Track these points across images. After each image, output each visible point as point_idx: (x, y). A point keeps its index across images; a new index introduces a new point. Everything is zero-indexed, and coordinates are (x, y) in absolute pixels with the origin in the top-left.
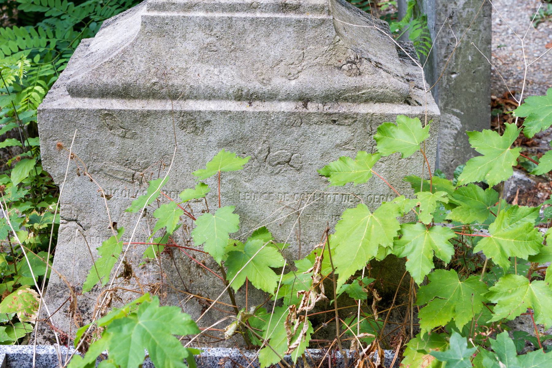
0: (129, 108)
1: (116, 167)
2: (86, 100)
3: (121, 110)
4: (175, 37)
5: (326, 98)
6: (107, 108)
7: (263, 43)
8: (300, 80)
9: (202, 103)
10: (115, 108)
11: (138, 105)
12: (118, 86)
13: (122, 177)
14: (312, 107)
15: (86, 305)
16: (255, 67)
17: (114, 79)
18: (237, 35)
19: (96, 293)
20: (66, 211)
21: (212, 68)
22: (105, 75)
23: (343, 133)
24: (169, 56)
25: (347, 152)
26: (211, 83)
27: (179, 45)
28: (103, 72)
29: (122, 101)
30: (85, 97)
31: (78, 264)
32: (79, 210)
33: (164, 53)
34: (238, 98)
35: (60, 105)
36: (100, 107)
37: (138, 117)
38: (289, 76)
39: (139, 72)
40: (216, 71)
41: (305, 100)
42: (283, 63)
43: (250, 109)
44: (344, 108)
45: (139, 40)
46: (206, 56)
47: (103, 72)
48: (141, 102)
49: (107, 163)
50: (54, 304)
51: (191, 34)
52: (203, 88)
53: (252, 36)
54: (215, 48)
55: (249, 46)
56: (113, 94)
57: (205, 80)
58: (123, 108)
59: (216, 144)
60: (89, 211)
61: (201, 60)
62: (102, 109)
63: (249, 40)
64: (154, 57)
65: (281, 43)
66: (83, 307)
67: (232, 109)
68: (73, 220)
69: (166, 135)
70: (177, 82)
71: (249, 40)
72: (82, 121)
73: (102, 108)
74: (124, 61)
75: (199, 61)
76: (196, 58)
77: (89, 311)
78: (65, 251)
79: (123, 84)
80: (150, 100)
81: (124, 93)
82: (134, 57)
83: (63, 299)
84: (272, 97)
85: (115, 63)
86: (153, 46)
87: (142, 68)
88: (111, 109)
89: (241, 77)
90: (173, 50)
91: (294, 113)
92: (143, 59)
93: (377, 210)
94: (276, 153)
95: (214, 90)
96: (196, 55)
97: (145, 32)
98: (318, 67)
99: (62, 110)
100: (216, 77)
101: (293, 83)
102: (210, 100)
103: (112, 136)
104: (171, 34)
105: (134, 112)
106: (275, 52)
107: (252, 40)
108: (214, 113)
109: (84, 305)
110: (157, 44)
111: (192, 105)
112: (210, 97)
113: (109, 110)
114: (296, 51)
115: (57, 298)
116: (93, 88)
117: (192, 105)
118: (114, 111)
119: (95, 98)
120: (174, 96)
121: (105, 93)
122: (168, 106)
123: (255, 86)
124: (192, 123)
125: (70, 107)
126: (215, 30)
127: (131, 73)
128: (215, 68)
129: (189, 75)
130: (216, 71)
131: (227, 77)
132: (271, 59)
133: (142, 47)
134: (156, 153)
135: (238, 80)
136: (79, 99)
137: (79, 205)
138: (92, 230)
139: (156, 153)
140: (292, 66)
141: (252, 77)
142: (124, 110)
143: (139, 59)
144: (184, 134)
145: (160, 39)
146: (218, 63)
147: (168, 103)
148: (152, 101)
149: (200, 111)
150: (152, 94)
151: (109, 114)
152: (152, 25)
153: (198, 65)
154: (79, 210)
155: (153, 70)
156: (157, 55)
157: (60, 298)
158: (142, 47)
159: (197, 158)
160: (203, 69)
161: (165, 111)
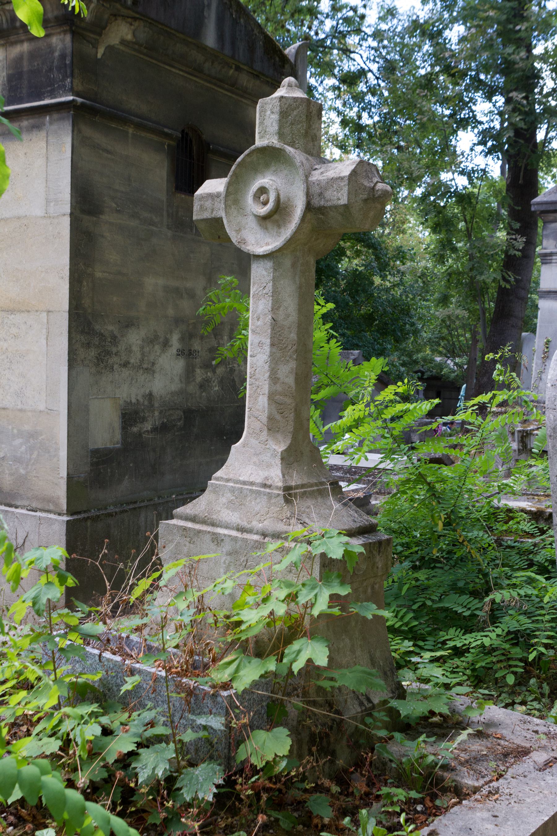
7: (253, 503)
11: (197, 527)
34: (238, 530)
61: (227, 508)
70: (214, 517)
89: (240, 518)
106: (257, 508)
112: (227, 527)
120: (213, 525)
123: (245, 524)
124: (217, 540)
131: (233, 517)
135: (238, 520)
146: (234, 510)
150: (204, 522)
156: (211, 502)
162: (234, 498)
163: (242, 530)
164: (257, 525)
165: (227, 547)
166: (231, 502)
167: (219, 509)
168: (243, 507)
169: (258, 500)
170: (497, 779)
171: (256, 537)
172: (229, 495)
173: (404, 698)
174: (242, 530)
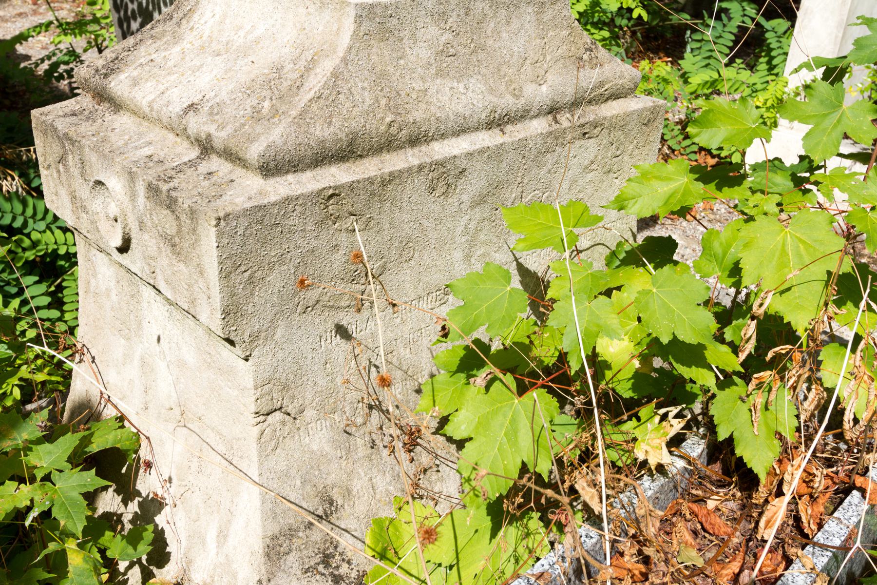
0: (363, 177)
1: (341, 287)
2: (290, 177)
3: (353, 182)
4: (402, 39)
5: (575, 104)
6: (332, 184)
7: (505, 35)
8: (550, 83)
9: (450, 144)
10: (344, 182)
11: (369, 168)
12: (341, 140)
13: (347, 303)
14: (564, 119)
15: (331, 543)
16: (502, 73)
17: (332, 129)
18: (475, 25)
19: (338, 515)
20: (263, 400)
21: (455, 84)
22: (318, 124)
23: (590, 149)
24: (398, 74)
25: (592, 174)
26: (460, 108)
27: (409, 51)
28: (311, 118)
29: (344, 166)
30: (287, 172)
31: (298, 482)
32: (285, 387)
33: (392, 70)
34: (490, 125)
35: (250, 198)
36: (320, 186)
37: (375, 187)
38: (539, 81)
39: (366, 108)
40: (461, 86)
41: (553, 111)
42: (528, 62)
43: (507, 139)
44: (592, 113)
45: (354, 51)
46: (445, 65)
47: (311, 118)
48: (372, 162)
49: (327, 285)
50: (284, 571)
51: (422, 30)
52: (452, 117)
53: (492, 25)
54: (452, 51)
55: (490, 42)
56: (332, 156)
57: (453, 105)
58: (355, 179)
59: (469, 204)
60: (300, 382)
61: (440, 73)
62: (324, 189)
63: (489, 32)
64: (380, 78)
65: (523, 31)
66: (328, 548)
67: (487, 143)
68: (275, 410)
69: (414, 205)
70: (418, 115)
71: (489, 32)
72: (294, 219)
73: (323, 186)
74: (339, 93)
75: (437, 74)
76: (433, 71)
77: (338, 549)
78: (273, 471)
79: (347, 135)
80: (384, 155)
81: (347, 152)
82: (352, 81)
83: (294, 553)
84: (524, 115)
85: (327, 99)
86: (375, 58)
87: (368, 102)
88: (338, 184)
89: (491, 90)
90: (402, 62)
91: (551, 133)
92: (366, 84)
93: (217, 279)
94: (529, 197)
95: (465, 118)
96: (432, 65)
97: (361, 34)
98: (562, 61)
99: (260, 208)
100: (463, 97)
101: (544, 88)
102: (458, 135)
103: (337, 234)
104: (396, 33)
105: (371, 181)
106: (518, 47)
107: (492, 32)
108: (471, 154)
109: (328, 544)
110: (379, 53)
111: (440, 150)
112: (462, 131)
113: (335, 188)
114: (538, 41)
115: (284, 558)
116: (302, 153)
117: (440, 150)
118: (342, 186)
119: (303, 170)
120: (414, 141)
121: (321, 158)
122: (408, 158)
123: (508, 103)
124: (444, 176)
125: (273, 199)
126: (450, 20)
127: (354, 113)
128: (458, 82)
129: (431, 100)
130: (461, 86)
131: (467, 96)
132: (515, 58)
133: (360, 63)
134: (396, 244)
135: (490, 97)
136: (278, 179)
137: (283, 379)
138: (309, 413)
139: (396, 244)
140: (538, 65)
141: (503, 88)
142: (358, 182)
143: (360, 85)
144: (433, 200)
145: (382, 44)
146: (462, 75)
147: (409, 155)
148: (386, 156)
149: (455, 157)
150: (388, 144)
151: (333, 195)
152: (370, 20)
153: (438, 81)
154: (285, 387)
155: (383, 102)
156: (384, 75)
157: (288, 553)
158: (360, 63)
159: (446, 234)
160: (446, 85)
161: (411, 168)
162: (448, 36)
163: (499, 121)
164: (541, 93)
165: (474, 184)
166: (445, 52)
167: (418, 85)
168: (481, 55)
169: (515, 24)
170: (707, 97)
171: (539, 126)
172: (433, 30)
173: (754, 220)
174: (499, 121)
